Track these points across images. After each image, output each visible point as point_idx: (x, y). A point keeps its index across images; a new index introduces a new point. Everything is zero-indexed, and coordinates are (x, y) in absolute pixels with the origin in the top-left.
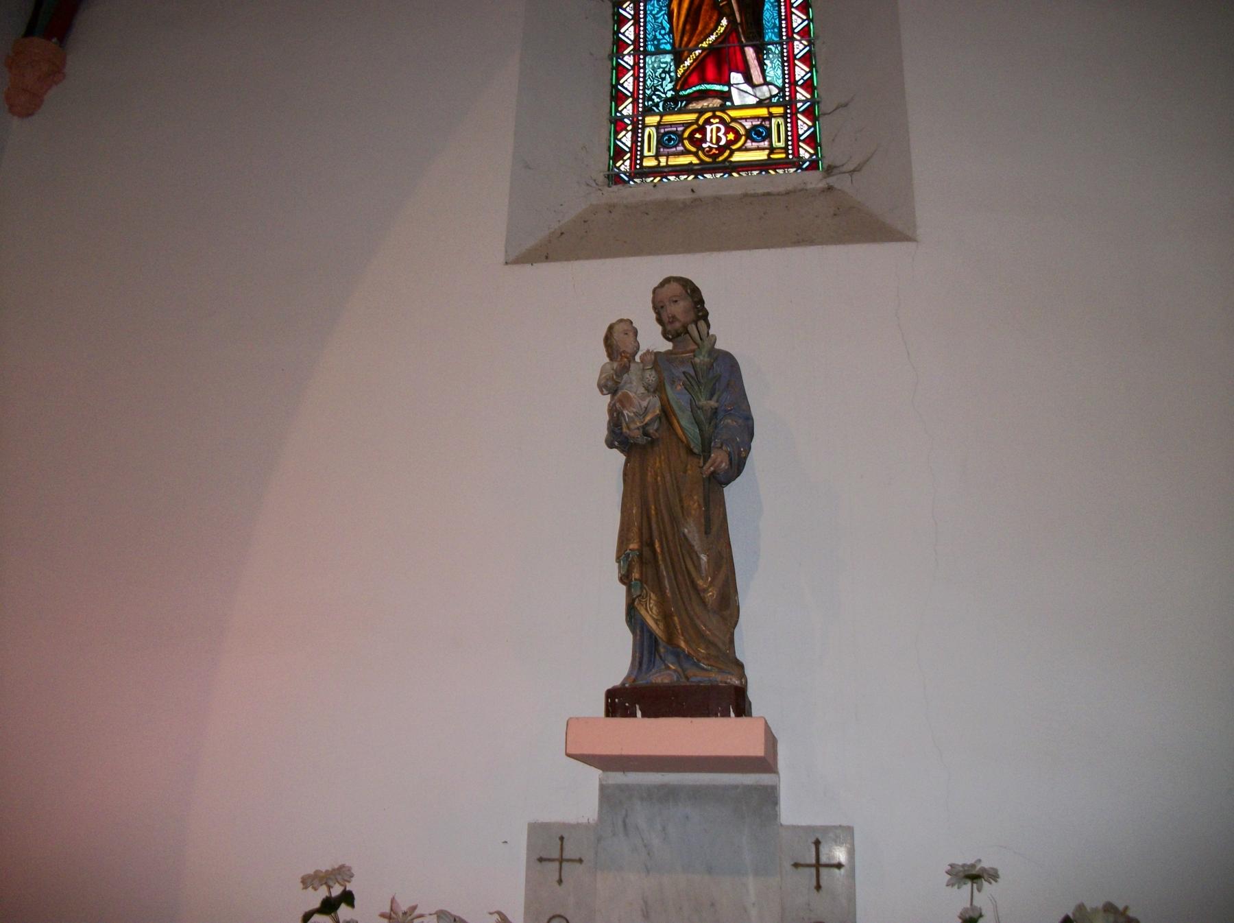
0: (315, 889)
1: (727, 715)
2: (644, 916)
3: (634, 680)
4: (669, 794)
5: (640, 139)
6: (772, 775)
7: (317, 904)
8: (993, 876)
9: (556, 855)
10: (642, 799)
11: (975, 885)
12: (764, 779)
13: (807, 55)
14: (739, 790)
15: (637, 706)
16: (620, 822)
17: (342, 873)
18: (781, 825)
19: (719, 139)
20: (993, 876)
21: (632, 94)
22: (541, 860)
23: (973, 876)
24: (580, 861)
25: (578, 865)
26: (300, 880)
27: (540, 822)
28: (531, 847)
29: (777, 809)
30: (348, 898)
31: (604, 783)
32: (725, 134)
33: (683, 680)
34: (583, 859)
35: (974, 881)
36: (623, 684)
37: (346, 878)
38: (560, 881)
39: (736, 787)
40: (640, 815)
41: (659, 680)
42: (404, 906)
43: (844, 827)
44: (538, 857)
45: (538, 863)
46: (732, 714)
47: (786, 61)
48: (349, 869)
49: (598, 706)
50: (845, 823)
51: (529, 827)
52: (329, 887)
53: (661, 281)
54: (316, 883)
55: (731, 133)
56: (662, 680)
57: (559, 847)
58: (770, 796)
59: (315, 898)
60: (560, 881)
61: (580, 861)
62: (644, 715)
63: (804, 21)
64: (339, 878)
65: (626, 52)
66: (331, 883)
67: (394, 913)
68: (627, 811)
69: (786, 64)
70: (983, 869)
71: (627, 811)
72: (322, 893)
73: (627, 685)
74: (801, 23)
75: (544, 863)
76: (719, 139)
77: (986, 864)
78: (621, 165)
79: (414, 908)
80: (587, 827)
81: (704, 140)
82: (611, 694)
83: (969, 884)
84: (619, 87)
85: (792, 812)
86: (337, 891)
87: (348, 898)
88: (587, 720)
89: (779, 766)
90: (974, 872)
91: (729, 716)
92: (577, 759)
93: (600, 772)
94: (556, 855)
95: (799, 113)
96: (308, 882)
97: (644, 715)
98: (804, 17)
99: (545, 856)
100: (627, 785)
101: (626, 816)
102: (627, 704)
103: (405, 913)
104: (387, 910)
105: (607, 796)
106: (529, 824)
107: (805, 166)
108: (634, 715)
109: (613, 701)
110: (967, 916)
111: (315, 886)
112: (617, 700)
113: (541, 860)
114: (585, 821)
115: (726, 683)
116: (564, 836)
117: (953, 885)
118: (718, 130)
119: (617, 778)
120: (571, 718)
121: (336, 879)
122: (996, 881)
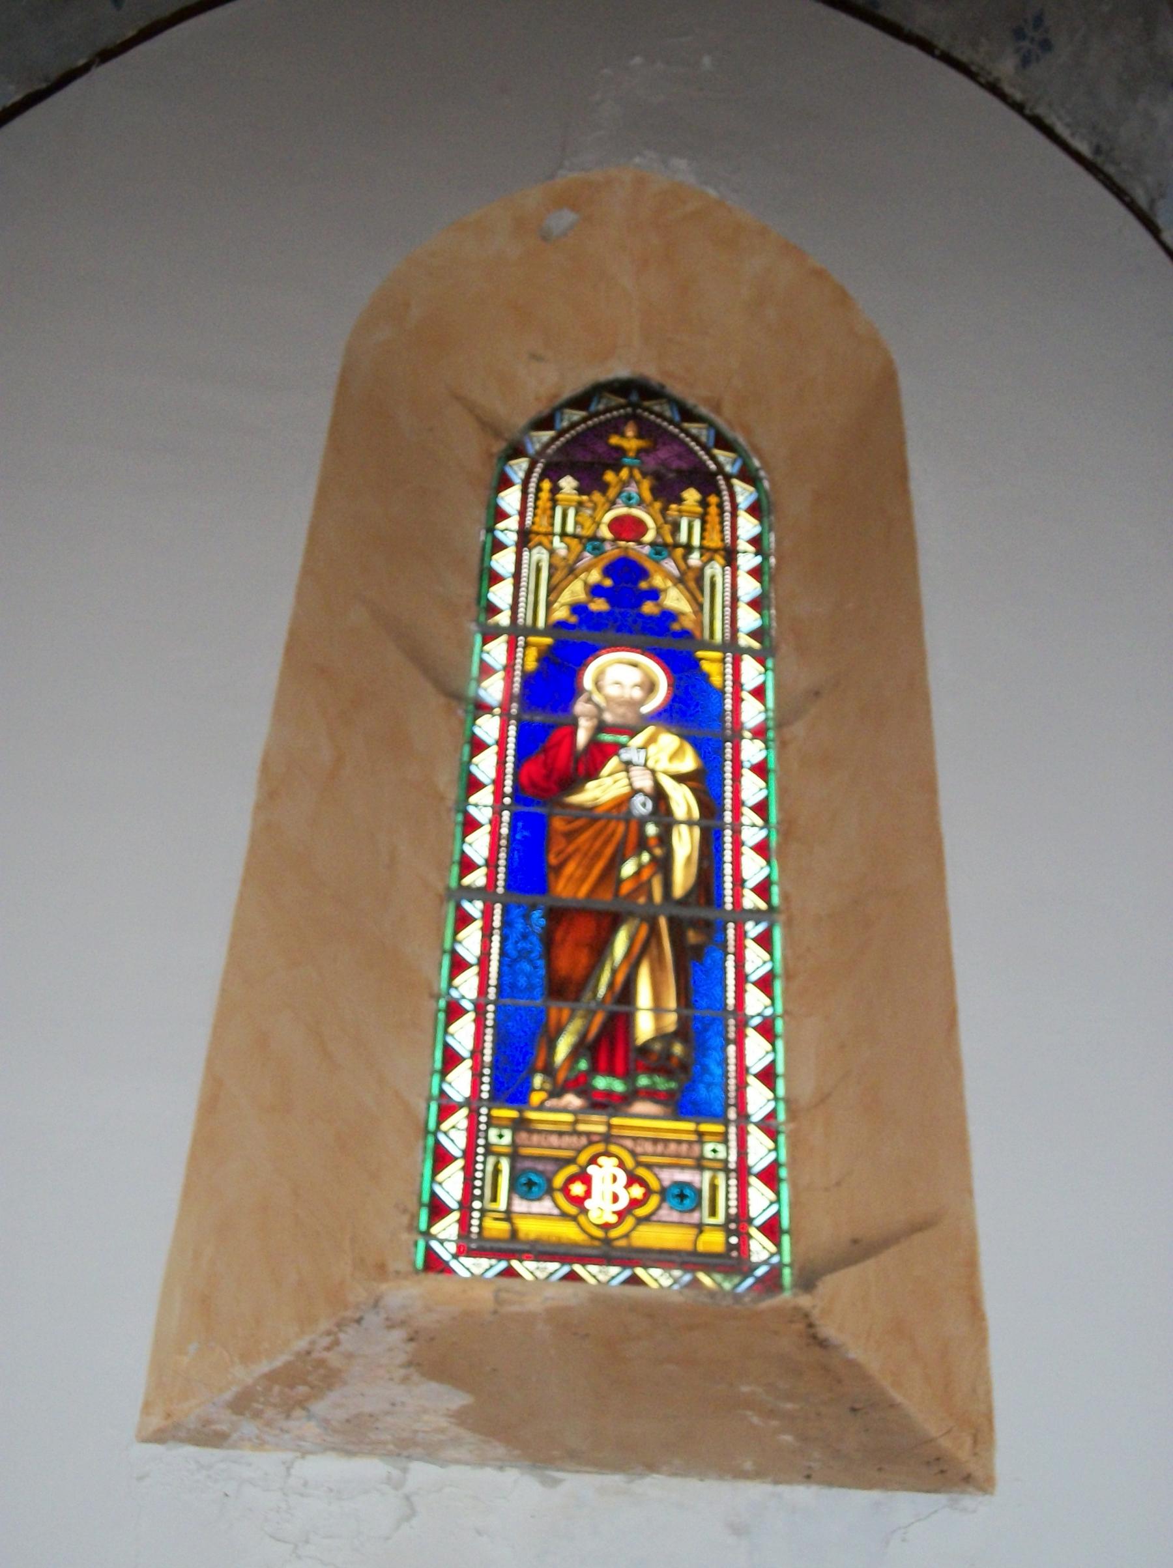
32: (629, 1185)
76: (615, 1198)
81: (588, 1194)
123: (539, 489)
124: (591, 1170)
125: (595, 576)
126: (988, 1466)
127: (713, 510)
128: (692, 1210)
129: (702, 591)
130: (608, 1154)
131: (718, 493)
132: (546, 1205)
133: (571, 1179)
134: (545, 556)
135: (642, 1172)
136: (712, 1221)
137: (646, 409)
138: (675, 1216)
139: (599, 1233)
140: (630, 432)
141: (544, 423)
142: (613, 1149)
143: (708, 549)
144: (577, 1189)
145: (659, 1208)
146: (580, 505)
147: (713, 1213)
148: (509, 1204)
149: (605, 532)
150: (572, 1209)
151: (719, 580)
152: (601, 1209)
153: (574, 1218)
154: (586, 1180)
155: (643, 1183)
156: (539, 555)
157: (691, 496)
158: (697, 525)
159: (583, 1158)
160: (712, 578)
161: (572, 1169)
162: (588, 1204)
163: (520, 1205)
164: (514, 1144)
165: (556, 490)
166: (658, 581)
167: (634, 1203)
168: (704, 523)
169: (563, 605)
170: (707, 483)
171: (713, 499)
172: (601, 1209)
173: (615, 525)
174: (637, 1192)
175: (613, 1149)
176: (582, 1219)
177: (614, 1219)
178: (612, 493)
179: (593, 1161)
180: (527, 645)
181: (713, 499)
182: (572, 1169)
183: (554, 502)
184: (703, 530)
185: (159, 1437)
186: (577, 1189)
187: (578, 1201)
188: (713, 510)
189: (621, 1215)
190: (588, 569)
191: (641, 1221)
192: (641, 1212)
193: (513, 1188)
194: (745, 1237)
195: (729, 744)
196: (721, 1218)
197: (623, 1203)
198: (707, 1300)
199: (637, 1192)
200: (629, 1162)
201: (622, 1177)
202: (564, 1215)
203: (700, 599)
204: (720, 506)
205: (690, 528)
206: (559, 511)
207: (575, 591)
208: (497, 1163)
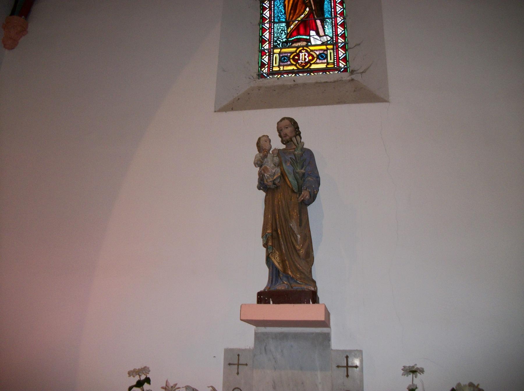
0: (134, 377)
1: (309, 303)
2: (273, 388)
3: (269, 288)
4: (284, 336)
5: (272, 59)
6: (328, 328)
7: (134, 383)
8: (422, 371)
9: (236, 362)
10: (273, 338)
11: (414, 375)
12: (325, 330)
13: (343, 23)
14: (314, 335)
15: (271, 299)
16: (263, 348)
17: (145, 370)
18: (332, 349)
19: (305, 59)
20: (422, 371)
21: (269, 40)
22: (230, 364)
23: (413, 371)
24: (246, 365)
25: (245, 366)
26: (127, 373)
27: (229, 348)
28: (225, 359)
29: (330, 343)
30: (148, 380)
31: (257, 332)
32: (308, 57)
33: (290, 288)
34: (248, 364)
35: (414, 373)
36: (265, 290)
37: (147, 372)
38: (238, 373)
39: (313, 333)
40: (272, 345)
41: (280, 288)
42: (171, 384)
43: (359, 350)
44: (229, 363)
45: (229, 365)
46: (311, 303)
47: (334, 26)
48: (148, 368)
49: (254, 299)
50: (359, 349)
51: (224, 350)
52: (140, 376)
53: (281, 119)
54: (134, 374)
55: (310, 56)
56: (281, 288)
57: (237, 359)
58: (327, 337)
59: (134, 380)
60: (238, 373)
61: (246, 365)
62: (273, 303)
63: (341, 9)
64: (144, 372)
65: (266, 22)
66: (140, 374)
67: (167, 387)
68: (266, 343)
69: (334, 27)
70: (418, 368)
71: (266, 343)
72: (137, 378)
73: (266, 290)
74: (340, 10)
75: (231, 366)
76: (305, 59)
77: (419, 366)
78: (264, 70)
79: (176, 385)
80: (249, 350)
81: (299, 59)
82: (259, 294)
83: (412, 375)
84: (263, 37)
85: (336, 344)
86: (143, 377)
87: (148, 380)
88: (249, 305)
89: (331, 325)
90: (414, 369)
91: (310, 303)
92: (245, 322)
93: (255, 327)
94: (236, 362)
95: (339, 48)
96: (131, 373)
97: (273, 303)
98: (342, 7)
99: (231, 363)
100: (266, 333)
101: (266, 346)
102: (266, 298)
103: (172, 387)
104: (164, 385)
105: (258, 337)
106: (225, 349)
107: (342, 70)
108: (269, 303)
109: (260, 297)
110: (411, 388)
111: (134, 375)
112: (262, 297)
113: (230, 364)
114: (248, 348)
115: (308, 289)
116: (239, 354)
117: (405, 375)
118: (305, 55)
119: (262, 330)
120: (242, 304)
121: (143, 372)
122: (423, 373)
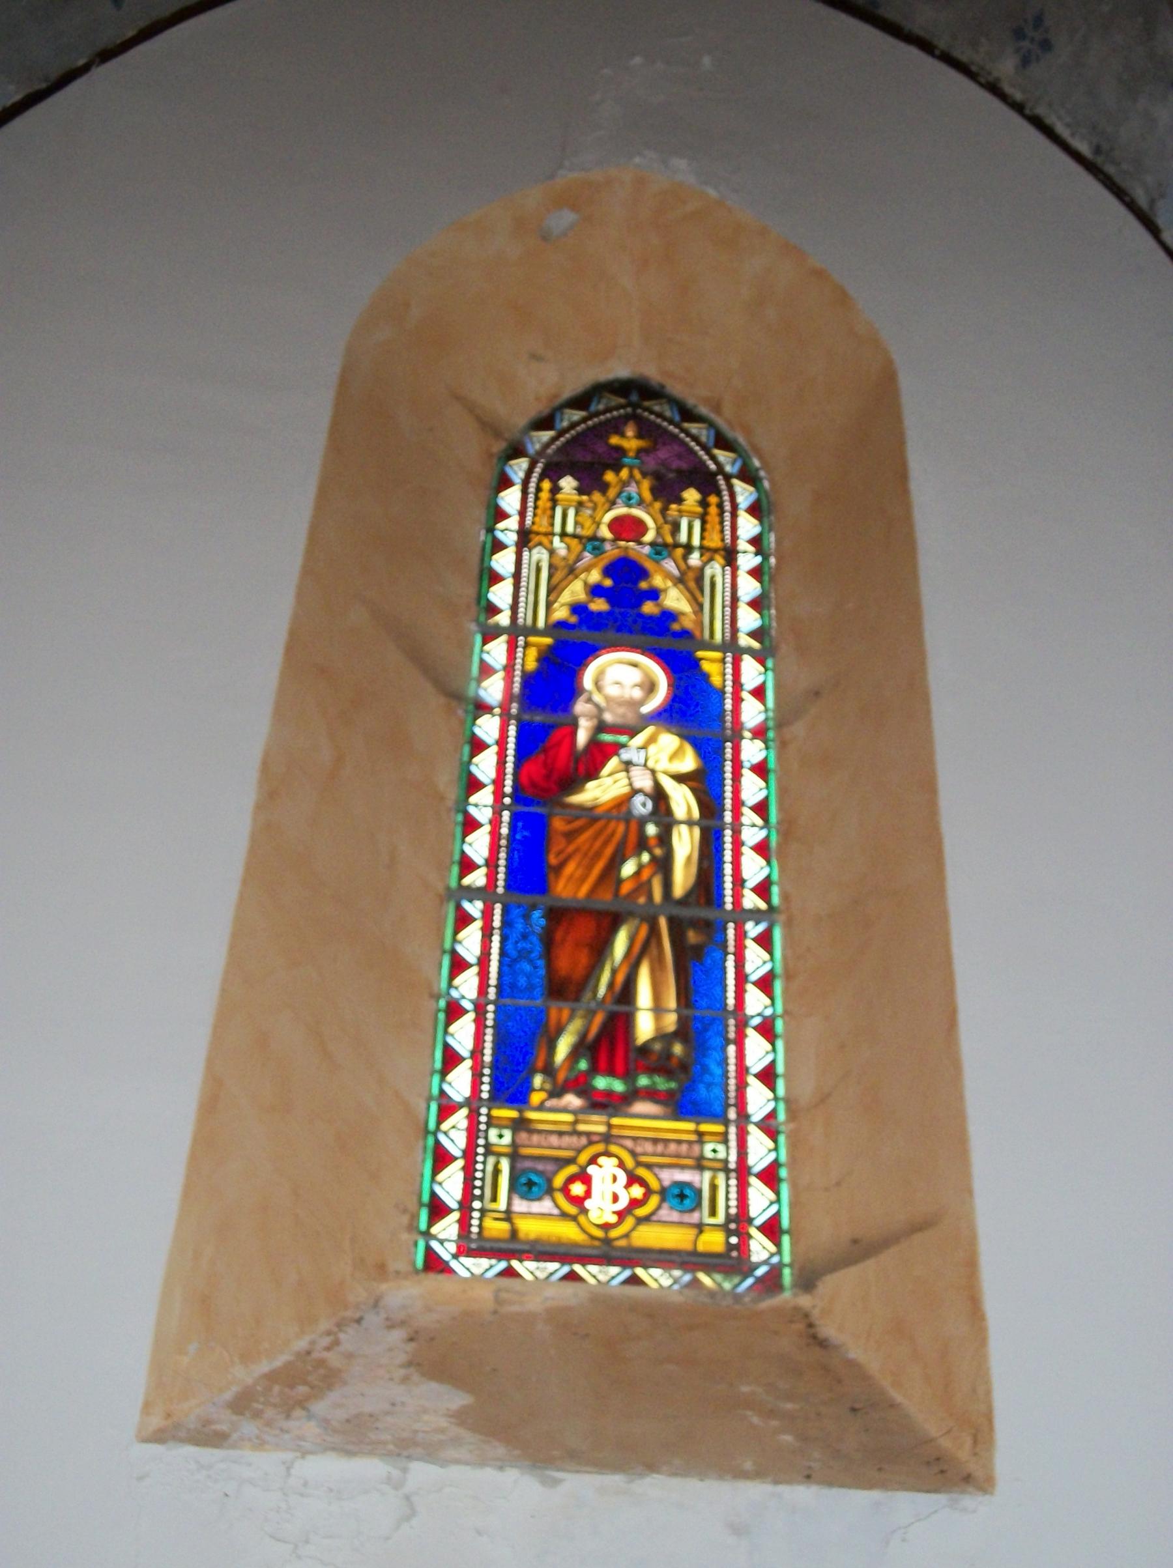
32: (629, 1185)
76: (615, 1198)
81: (588, 1194)
123: (539, 489)
124: (591, 1170)
125: (595, 576)
126: (988, 1466)
127: (713, 510)
128: (692, 1210)
129: (702, 591)
130: (608, 1154)
131: (718, 493)
132: (546, 1205)
133: (571, 1179)
134: (545, 556)
135: (642, 1172)
136: (712, 1221)
137: (646, 409)
138: (675, 1216)
139: (599, 1233)
140: (630, 432)
141: (544, 423)
142: (613, 1149)
143: (708, 549)
144: (577, 1189)
145: (659, 1208)
146: (580, 505)
147: (713, 1213)
148: (509, 1204)
149: (605, 532)
150: (572, 1209)
151: (719, 580)
152: (601, 1209)
153: (574, 1218)
154: (586, 1180)
155: (643, 1183)
156: (539, 555)
157: (691, 496)
158: (697, 525)
159: (583, 1158)
160: (712, 578)
161: (572, 1169)
162: (588, 1204)
163: (520, 1205)
164: (514, 1144)
165: (556, 490)
166: (658, 581)
167: (634, 1203)
168: (704, 523)
169: (563, 605)
170: (707, 483)
171: (713, 499)
172: (601, 1209)
173: (615, 525)
174: (637, 1192)
175: (613, 1149)
176: (582, 1219)
177: (614, 1219)
178: (612, 493)
179: (593, 1161)
180: (527, 645)
181: (713, 499)
182: (572, 1169)
183: (554, 502)
184: (703, 530)
185: (159, 1437)
186: (577, 1189)
187: (578, 1201)
188: (713, 510)
189: (621, 1215)
190: (588, 569)
191: (641, 1221)
192: (641, 1212)
193: (513, 1188)
194: (745, 1237)
195: (729, 744)
196: (721, 1218)
197: (623, 1203)
198: (707, 1300)
199: (637, 1192)
200: (629, 1162)
201: (622, 1177)
202: (564, 1215)
203: (700, 599)
204: (720, 506)
205: (690, 528)
206: (559, 511)
207: (575, 591)
208: (497, 1163)
